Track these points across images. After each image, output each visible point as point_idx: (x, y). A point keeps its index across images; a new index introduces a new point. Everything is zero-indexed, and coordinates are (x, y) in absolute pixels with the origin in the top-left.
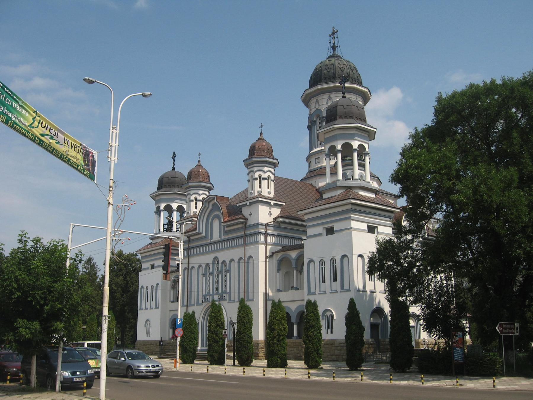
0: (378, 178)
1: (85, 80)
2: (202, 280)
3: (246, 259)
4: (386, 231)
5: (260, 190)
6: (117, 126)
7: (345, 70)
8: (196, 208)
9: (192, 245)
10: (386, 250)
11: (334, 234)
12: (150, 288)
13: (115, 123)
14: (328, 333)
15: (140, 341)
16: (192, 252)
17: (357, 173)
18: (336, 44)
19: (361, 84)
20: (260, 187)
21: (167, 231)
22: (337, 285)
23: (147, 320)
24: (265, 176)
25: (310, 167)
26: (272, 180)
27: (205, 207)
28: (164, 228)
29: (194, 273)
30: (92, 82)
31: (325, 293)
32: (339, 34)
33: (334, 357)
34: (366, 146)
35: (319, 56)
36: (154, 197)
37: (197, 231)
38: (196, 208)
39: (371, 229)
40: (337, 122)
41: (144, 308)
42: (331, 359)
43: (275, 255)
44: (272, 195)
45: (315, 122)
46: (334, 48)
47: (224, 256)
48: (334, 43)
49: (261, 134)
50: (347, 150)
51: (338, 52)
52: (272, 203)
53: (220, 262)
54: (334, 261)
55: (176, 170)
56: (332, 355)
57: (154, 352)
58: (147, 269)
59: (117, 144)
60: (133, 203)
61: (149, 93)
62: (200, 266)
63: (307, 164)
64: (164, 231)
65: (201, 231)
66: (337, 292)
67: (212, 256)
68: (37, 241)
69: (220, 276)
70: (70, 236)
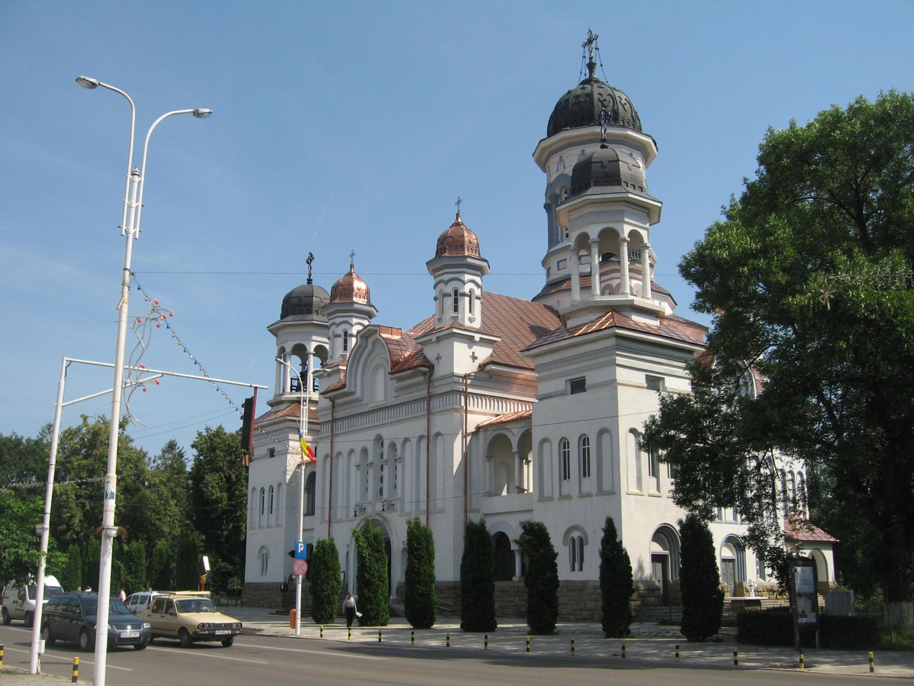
0: (670, 295)
1: (78, 79)
2: (355, 476)
3: (431, 438)
4: (679, 384)
6: (141, 169)
7: (611, 104)
8: (345, 349)
9: (339, 414)
10: (674, 412)
11: (585, 391)
13: (137, 163)
14: (573, 569)
17: (630, 283)
19: (639, 130)
20: (456, 309)
22: (590, 484)
23: (262, 547)
24: (467, 289)
25: (548, 275)
26: (478, 298)
28: (292, 386)
29: (342, 463)
30: (93, 85)
31: (569, 497)
32: (600, 43)
33: (584, 614)
34: (644, 233)
35: (569, 81)
36: (274, 330)
37: (346, 390)
38: (345, 349)
39: (654, 382)
40: (589, 192)
41: (257, 525)
42: (579, 617)
43: (481, 434)
44: (477, 324)
46: (591, 66)
48: (591, 58)
50: (610, 236)
51: (597, 74)
52: (477, 337)
53: (386, 444)
54: (584, 440)
55: (314, 283)
56: (582, 610)
58: (261, 458)
59: (140, 204)
60: (167, 315)
61: (208, 111)
62: (352, 451)
63: (544, 271)
64: (291, 390)
65: (353, 390)
69: (386, 468)
70: (63, 381)
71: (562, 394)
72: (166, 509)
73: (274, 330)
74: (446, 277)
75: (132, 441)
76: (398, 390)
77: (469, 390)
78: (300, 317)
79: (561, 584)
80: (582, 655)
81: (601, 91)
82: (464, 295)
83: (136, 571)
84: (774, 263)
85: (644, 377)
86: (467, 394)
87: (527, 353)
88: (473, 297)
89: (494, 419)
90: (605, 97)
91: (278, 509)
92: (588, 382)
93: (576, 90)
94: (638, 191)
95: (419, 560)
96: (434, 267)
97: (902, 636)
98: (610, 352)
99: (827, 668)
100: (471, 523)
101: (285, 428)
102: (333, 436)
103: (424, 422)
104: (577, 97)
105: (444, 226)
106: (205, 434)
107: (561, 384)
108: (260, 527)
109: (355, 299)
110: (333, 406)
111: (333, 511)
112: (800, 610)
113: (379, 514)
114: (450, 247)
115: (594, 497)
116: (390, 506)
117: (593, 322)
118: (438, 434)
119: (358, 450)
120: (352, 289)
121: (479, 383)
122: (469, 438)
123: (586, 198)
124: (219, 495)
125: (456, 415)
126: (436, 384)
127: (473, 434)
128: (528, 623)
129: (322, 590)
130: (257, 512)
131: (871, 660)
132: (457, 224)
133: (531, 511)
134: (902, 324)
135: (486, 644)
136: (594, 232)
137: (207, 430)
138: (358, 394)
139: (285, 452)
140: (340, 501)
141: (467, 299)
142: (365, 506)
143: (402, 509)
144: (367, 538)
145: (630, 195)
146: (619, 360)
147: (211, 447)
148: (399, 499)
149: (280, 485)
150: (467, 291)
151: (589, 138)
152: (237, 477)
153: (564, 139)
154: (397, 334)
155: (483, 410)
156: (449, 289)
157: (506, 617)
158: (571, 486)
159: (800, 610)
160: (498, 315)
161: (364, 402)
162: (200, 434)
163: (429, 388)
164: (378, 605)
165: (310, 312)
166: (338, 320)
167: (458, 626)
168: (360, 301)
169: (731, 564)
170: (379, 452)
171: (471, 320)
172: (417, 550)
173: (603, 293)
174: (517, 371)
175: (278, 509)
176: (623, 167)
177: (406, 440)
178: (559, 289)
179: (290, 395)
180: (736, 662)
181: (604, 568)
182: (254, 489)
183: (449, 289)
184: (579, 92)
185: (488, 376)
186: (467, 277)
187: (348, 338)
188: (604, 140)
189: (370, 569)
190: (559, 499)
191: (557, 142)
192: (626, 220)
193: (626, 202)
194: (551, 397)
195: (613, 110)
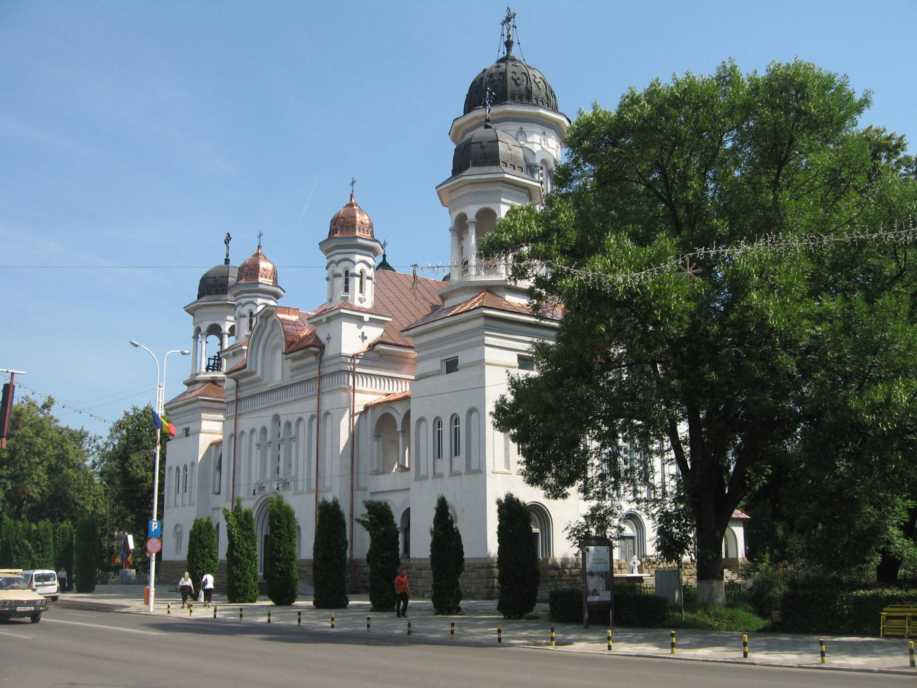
2: (256, 454)
5: (360, 295)
7: (525, 83)
9: (242, 395)
12: (181, 469)
15: (166, 562)
16: (245, 406)
19: (555, 109)
20: (347, 290)
21: (213, 370)
22: (460, 463)
23: (177, 526)
24: (357, 270)
26: (369, 278)
29: (244, 443)
32: (517, 21)
35: (486, 59)
36: (191, 310)
37: (247, 370)
40: (467, 172)
43: (369, 410)
46: (509, 44)
47: (289, 413)
48: (509, 36)
51: (515, 52)
53: (283, 424)
62: (253, 431)
65: (253, 370)
66: (461, 474)
67: (271, 412)
68: (134, 409)
69: (282, 447)
71: (437, 373)
72: (89, 489)
73: (191, 310)
74: (337, 258)
75: (57, 421)
76: (293, 370)
77: (357, 370)
78: (215, 297)
79: (466, 562)
80: (379, 631)
81: (515, 69)
82: (354, 275)
83: (43, 550)
84: (554, 247)
85: (516, 358)
86: (354, 374)
87: (406, 333)
89: (384, 398)
90: (519, 75)
91: (191, 487)
92: (461, 362)
93: (491, 68)
95: (280, 538)
96: (327, 247)
97: (708, 614)
98: (479, 332)
99: (585, 646)
100: (325, 502)
101: (197, 408)
103: (315, 401)
104: (491, 75)
105: (338, 208)
106: (131, 414)
107: (436, 364)
108: (176, 505)
109: (260, 280)
110: (237, 386)
111: (236, 488)
112: (591, 589)
113: (274, 493)
114: (342, 227)
115: (463, 475)
117: (467, 302)
118: (327, 414)
119: (258, 429)
120: (258, 270)
121: (369, 363)
122: (356, 418)
123: (463, 178)
124: (144, 473)
125: (344, 395)
126: (326, 364)
127: (361, 413)
128: (371, 600)
129: (198, 568)
130: (173, 491)
131: (609, 638)
132: (351, 205)
133: (408, 489)
134: (659, 307)
135: (299, 620)
136: (471, 212)
137: (134, 409)
138: (259, 374)
139: (199, 432)
140: (242, 479)
141: (357, 280)
143: (296, 486)
144: (237, 517)
145: (506, 176)
146: (488, 340)
149: (193, 464)
150: (357, 271)
151: (501, 116)
153: (475, 118)
154: (296, 314)
155: (373, 389)
156: (340, 270)
157: (356, 592)
158: (443, 465)
159: (591, 589)
160: (399, 294)
161: (264, 382)
162: (127, 414)
163: (319, 368)
164: (246, 582)
165: (225, 292)
166: (243, 301)
167: (311, 603)
168: (265, 281)
169: (631, 541)
171: (361, 300)
172: (278, 528)
173: (478, 274)
174: (407, 351)
175: (191, 487)
176: (502, 147)
180: (500, 639)
181: (435, 546)
182: (170, 468)
183: (340, 270)
184: (494, 70)
185: (376, 355)
186: (358, 258)
187: (350, 278)
188: (488, 120)
190: (433, 478)
192: (503, 200)
193: (503, 182)
194: (427, 377)
195: (527, 88)
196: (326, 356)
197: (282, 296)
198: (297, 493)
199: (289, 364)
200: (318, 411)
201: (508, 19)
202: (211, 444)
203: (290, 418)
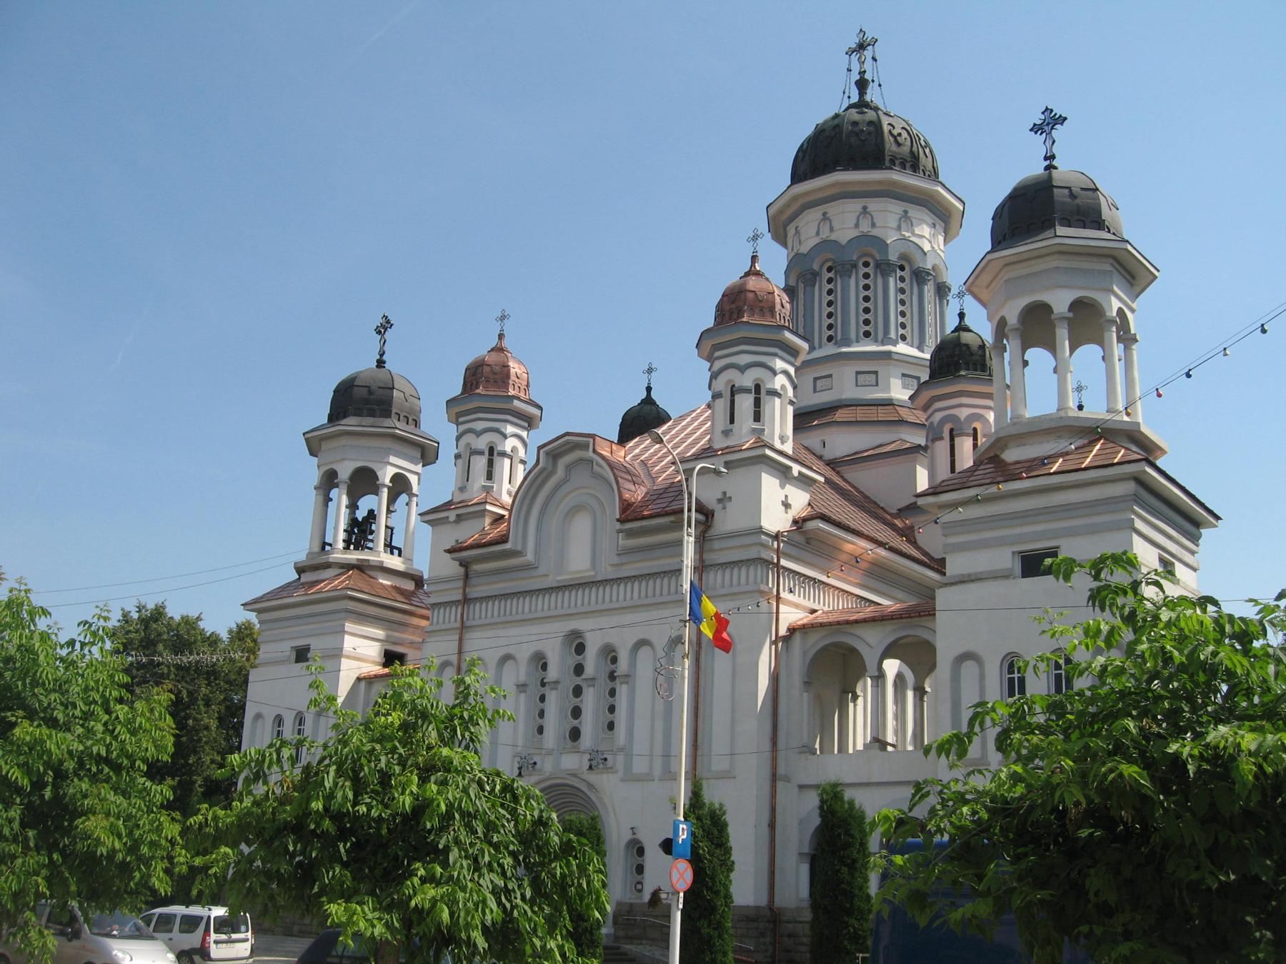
7: (908, 143)
9: (475, 592)
16: (478, 612)
18: (868, 76)
20: (490, 476)
27: (544, 469)
34: (413, 479)
35: (827, 101)
36: (314, 443)
37: (508, 546)
40: (344, 422)
43: (798, 635)
45: (815, 275)
46: (862, 85)
48: (862, 73)
49: (501, 336)
52: (796, 469)
57: (296, 928)
62: (507, 658)
65: (519, 548)
71: (1005, 575)
77: (783, 562)
78: (370, 420)
82: (503, 454)
88: (516, 460)
94: (411, 428)
102: (463, 628)
105: (480, 349)
107: (1005, 559)
110: (467, 576)
116: (598, 762)
120: (508, 376)
126: (716, 545)
136: (345, 471)
137: (140, 608)
138: (530, 557)
142: (536, 759)
147: (147, 638)
148: (621, 750)
152: (190, 694)
155: (801, 601)
161: (541, 571)
165: (387, 414)
166: (480, 426)
170: (573, 659)
174: (850, 537)
177: (643, 643)
178: (824, 420)
179: (340, 554)
185: (806, 537)
186: (510, 429)
187: (496, 459)
189: (712, 878)
191: (821, 189)
195: (912, 152)
196: (712, 532)
197: (1155, 277)
198: (630, 777)
199: (624, 542)
200: (460, 652)
201: (861, 47)
202: (359, 679)
203: (612, 638)
